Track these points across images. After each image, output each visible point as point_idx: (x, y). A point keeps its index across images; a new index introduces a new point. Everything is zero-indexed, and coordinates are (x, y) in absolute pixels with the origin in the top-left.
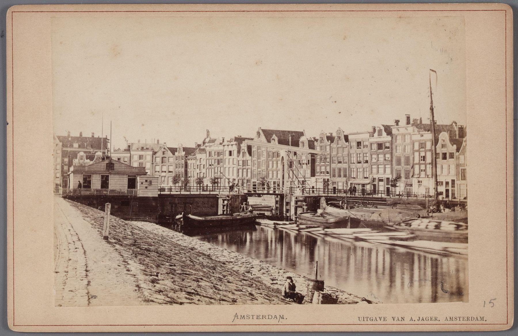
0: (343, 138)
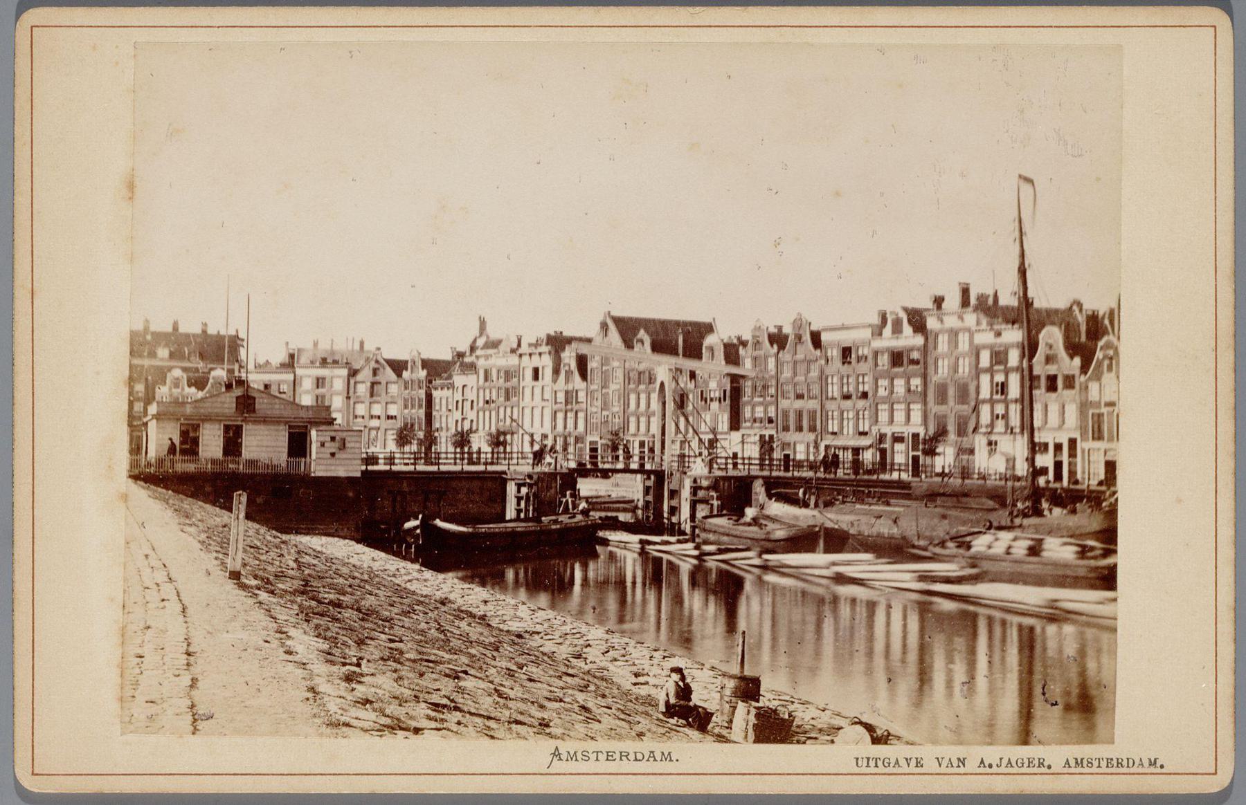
0: (807, 338)
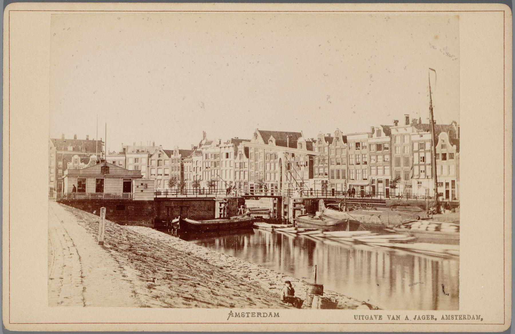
0: (341, 138)
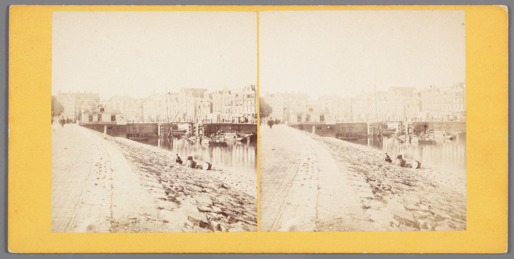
0: (228, 92)
